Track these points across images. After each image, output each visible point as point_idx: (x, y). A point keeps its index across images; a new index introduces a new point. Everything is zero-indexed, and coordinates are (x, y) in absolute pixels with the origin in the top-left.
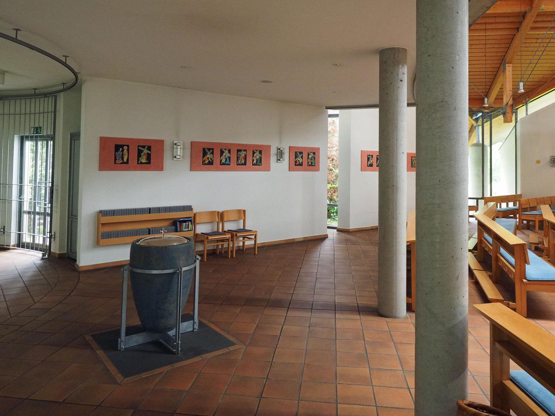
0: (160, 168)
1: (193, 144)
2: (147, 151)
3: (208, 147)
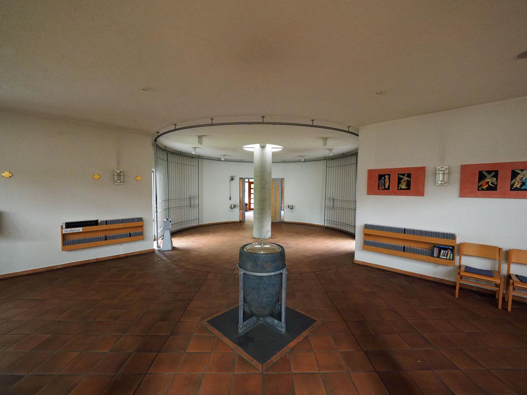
0: (420, 193)
1: (464, 168)
2: (407, 178)
3: (488, 170)
